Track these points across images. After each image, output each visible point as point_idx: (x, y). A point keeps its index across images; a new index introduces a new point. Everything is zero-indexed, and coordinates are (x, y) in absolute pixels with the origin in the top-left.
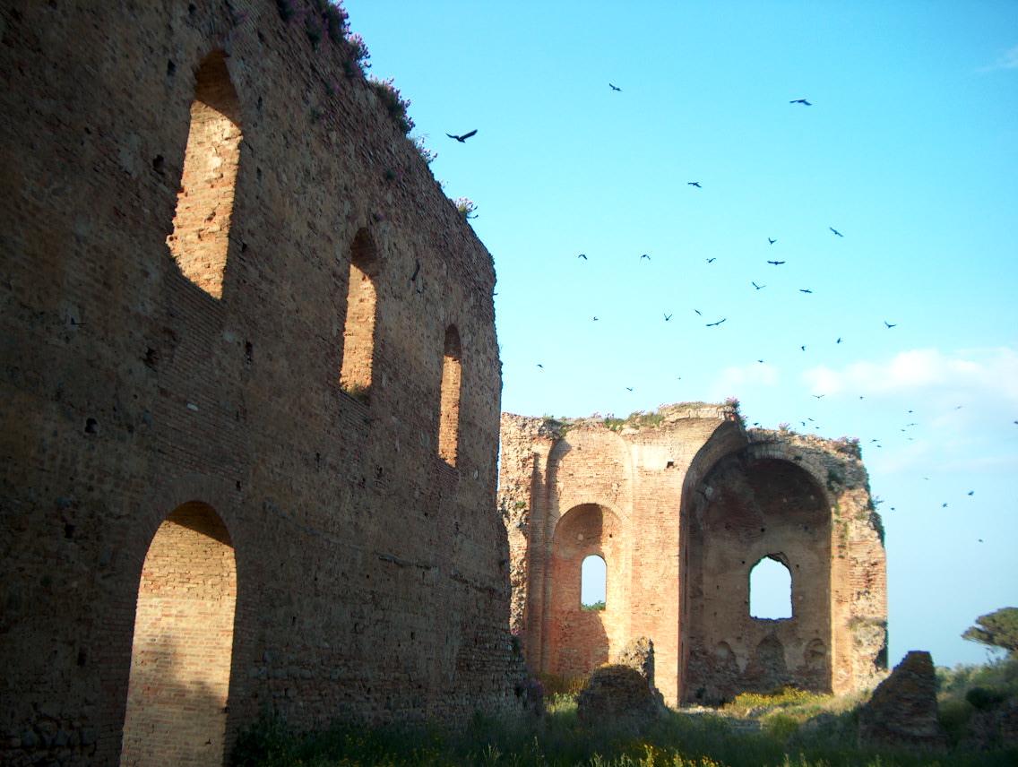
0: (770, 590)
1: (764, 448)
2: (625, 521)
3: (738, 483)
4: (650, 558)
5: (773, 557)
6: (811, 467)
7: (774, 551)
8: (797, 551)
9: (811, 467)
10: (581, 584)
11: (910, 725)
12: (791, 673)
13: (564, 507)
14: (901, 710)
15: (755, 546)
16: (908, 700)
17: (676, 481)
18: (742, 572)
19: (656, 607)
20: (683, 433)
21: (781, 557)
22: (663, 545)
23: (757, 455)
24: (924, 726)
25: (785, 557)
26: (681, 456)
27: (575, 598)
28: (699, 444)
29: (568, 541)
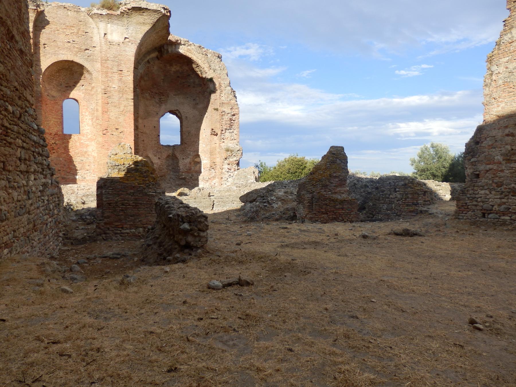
0: (169, 129)
1: (174, 47)
2: (95, 74)
3: (155, 68)
4: (116, 97)
5: (172, 112)
6: (200, 61)
7: (173, 108)
8: (186, 109)
9: (200, 61)
10: (62, 116)
11: (336, 193)
12: (183, 172)
13: (45, 62)
14: (332, 183)
15: (163, 107)
16: (336, 177)
17: (130, 52)
18: (156, 119)
19: (119, 130)
20: (137, 18)
21: (177, 112)
22: (121, 91)
23: (170, 50)
24: (343, 193)
25: (179, 112)
26: (134, 34)
27: (59, 125)
28: (147, 28)
29: (52, 87)
